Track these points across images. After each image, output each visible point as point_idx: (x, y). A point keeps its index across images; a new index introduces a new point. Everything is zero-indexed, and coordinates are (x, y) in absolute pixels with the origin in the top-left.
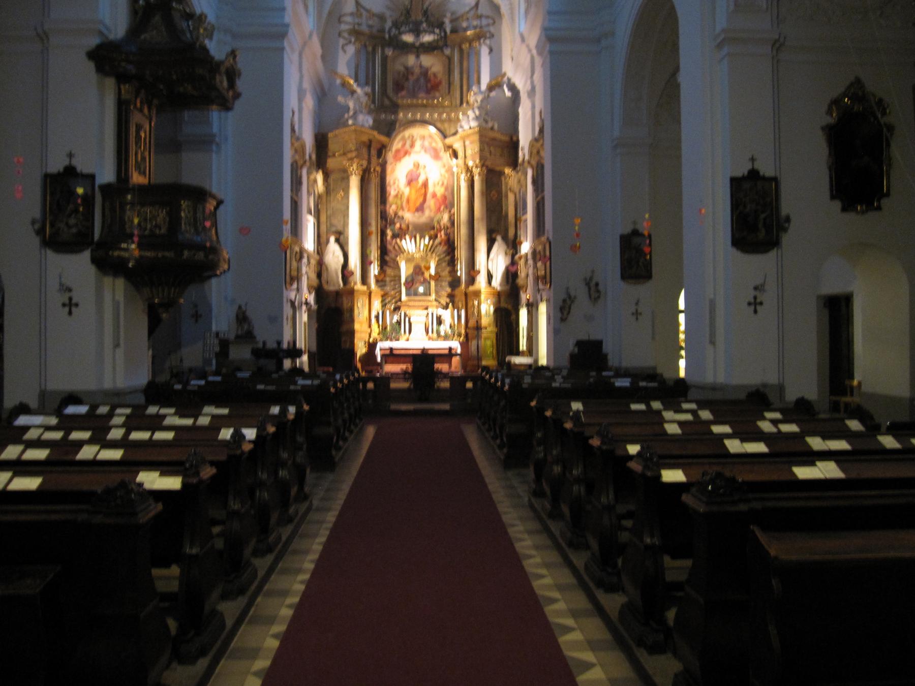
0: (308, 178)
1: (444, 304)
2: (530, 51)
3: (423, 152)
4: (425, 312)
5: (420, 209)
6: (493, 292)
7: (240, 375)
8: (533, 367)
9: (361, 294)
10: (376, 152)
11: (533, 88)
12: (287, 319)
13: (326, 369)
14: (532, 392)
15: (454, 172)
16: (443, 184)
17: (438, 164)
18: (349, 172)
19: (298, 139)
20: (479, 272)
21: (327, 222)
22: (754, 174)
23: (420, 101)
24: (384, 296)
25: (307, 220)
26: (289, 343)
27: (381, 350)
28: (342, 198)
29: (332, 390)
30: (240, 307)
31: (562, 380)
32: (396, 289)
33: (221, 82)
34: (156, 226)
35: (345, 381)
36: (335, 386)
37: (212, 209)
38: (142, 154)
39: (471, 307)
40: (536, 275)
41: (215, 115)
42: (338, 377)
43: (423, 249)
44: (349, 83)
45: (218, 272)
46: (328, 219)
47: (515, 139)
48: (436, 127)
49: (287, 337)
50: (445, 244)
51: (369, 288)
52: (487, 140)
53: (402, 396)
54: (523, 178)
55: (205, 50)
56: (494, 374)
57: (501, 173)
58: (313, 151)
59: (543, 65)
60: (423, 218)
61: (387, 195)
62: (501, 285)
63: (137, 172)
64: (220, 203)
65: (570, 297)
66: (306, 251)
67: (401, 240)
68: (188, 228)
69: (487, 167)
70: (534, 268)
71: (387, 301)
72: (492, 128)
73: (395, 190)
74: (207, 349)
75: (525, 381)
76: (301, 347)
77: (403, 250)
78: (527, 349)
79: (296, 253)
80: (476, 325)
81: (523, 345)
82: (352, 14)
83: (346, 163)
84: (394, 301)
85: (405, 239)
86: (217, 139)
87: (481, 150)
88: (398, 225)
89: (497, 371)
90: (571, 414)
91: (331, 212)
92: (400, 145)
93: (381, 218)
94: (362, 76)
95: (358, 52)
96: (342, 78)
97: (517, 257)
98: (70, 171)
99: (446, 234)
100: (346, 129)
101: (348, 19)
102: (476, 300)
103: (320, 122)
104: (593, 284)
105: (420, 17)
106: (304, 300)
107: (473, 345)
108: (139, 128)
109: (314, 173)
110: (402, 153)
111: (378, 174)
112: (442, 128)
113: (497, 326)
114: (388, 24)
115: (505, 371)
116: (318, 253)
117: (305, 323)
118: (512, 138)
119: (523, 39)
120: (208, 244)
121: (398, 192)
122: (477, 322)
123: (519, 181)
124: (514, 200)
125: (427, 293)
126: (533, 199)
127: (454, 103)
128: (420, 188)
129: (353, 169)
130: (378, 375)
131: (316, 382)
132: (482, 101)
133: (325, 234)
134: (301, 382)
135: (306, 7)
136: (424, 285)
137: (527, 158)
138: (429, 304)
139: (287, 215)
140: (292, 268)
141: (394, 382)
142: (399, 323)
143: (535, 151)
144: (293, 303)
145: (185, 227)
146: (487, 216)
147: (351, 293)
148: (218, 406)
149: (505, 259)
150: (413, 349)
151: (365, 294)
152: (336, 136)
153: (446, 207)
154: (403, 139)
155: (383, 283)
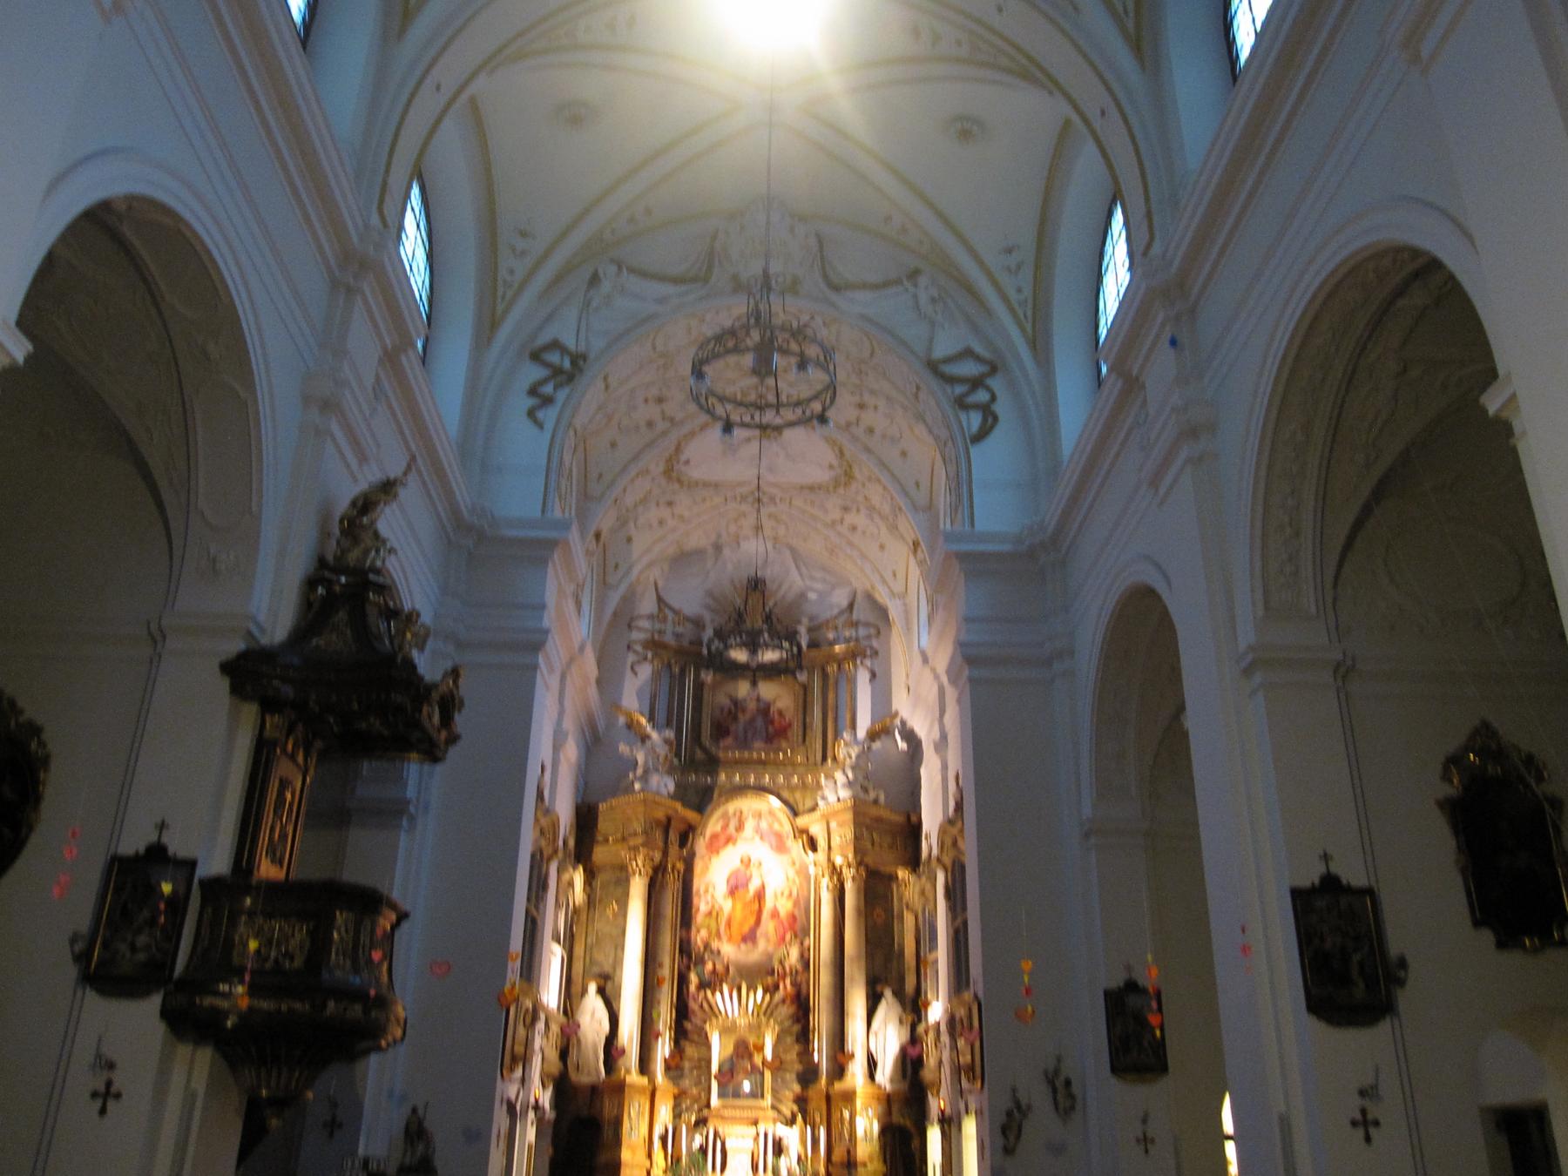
1: (788, 1113)
2: (937, 677)
3: (757, 838)
5: (750, 937)
16: (790, 895)
17: (784, 859)
19: (547, 812)
22: (1330, 883)
24: (678, 1099)
28: (615, 915)
33: (430, 717)
38: (283, 828)
41: (413, 769)
47: (914, 819)
50: (792, 1002)
51: (652, 1081)
52: (868, 821)
54: (928, 887)
57: (893, 878)
59: (959, 701)
60: (752, 955)
61: (694, 910)
62: (892, 1081)
63: (269, 860)
64: (403, 916)
65: (1019, 1106)
70: (951, 1049)
72: (876, 802)
73: (707, 903)
77: (717, 1012)
80: (846, 1160)
82: (651, 617)
83: (624, 854)
86: (412, 809)
87: (857, 838)
88: (709, 966)
92: (718, 828)
94: (661, 715)
95: (656, 676)
96: (629, 715)
98: (157, 854)
101: (645, 624)
103: (586, 783)
104: (1059, 1083)
105: (759, 623)
108: (284, 784)
112: (791, 800)
113: (885, 1161)
114: (709, 633)
119: (925, 660)
121: (713, 907)
123: (923, 893)
125: (757, 1094)
132: (858, 757)
137: (935, 852)
139: (516, 943)
142: (703, 1150)
143: (948, 842)
151: (644, 1093)
154: (726, 817)
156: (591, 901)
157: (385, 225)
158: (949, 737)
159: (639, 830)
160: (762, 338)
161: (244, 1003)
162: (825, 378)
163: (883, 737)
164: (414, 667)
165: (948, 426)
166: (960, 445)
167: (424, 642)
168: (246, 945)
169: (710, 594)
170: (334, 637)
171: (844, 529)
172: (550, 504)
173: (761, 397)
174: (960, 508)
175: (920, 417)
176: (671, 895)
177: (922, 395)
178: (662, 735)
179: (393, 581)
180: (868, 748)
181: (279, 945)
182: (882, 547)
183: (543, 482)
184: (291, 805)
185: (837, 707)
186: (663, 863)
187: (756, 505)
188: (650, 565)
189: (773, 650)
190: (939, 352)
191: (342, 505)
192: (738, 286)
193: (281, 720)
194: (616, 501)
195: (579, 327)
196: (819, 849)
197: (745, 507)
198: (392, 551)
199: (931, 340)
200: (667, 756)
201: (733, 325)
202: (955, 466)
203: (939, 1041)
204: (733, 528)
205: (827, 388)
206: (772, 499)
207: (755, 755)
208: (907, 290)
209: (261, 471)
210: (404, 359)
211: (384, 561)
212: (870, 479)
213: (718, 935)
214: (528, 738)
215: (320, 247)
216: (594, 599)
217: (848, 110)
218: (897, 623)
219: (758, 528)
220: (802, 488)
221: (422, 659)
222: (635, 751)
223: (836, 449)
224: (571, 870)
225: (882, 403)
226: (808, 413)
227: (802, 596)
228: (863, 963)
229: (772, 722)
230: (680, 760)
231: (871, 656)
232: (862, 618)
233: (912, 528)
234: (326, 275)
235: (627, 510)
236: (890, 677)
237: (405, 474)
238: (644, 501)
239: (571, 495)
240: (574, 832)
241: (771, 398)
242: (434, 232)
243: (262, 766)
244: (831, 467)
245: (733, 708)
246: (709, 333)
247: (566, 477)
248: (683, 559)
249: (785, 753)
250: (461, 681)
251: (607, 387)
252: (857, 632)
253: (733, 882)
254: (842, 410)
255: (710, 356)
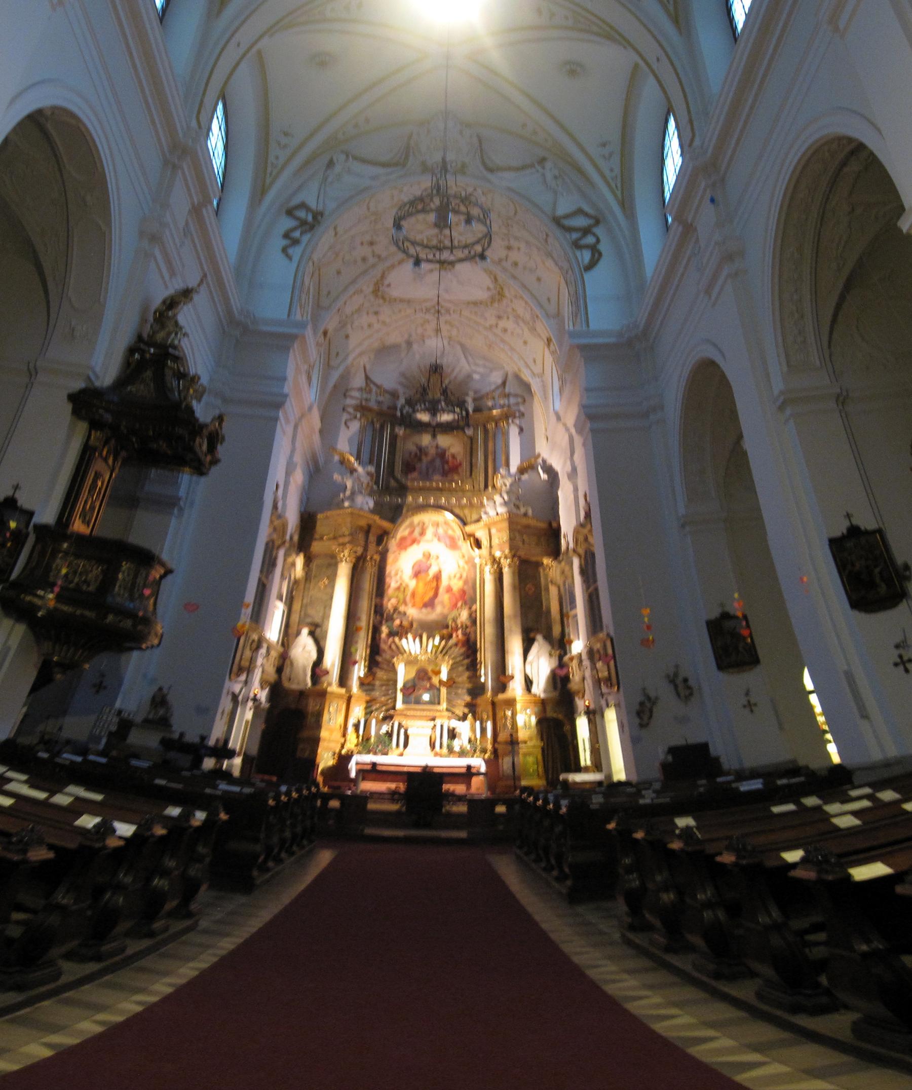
0: (285, 560)
1: (461, 714)
2: (567, 429)
3: (436, 540)
4: (432, 723)
5: (430, 604)
6: (535, 700)
7: (134, 762)
8: (605, 784)
9: (336, 697)
10: (375, 539)
11: (574, 469)
12: (223, 713)
13: (266, 777)
14: (607, 813)
15: (476, 564)
16: (461, 577)
17: (456, 554)
18: (338, 558)
19: (279, 517)
20: (512, 677)
21: (301, 611)
22: (854, 531)
23: (434, 484)
24: (369, 704)
25: (275, 607)
26: (218, 740)
27: (357, 764)
28: (326, 586)
29: (271, 802)
30: (160, 689)
31: (654, 795)
32: (388, 694)
33: (201, 446)
34: (85, 581)
35: (294, 795)
36: (277, 798)
37: (158, 576)
38: (93, 503)
39: (502, 718)
40: (597, 677)
41: (186, 478)
42: (284, 788)
43: (432, 651)
44: (348, 460)
45: (144, 646)
46: (303, 608)
47: (554, 525)
48: (452, 512)
49: (216, 733)
50: (463, 645)
51: (349, 690)
52: (519, 527)
53: (384, 819)
54: (567, 568)
55: (191, 412)
56: (541, 796)
57: (539, 564)
58: (295, 532)
59: (584, 445)
60: (432, 615)
61: (386, 587)
62: (545, 691)
63: (81, 520)
64: (168, 572)
65: (649, 698)
66: (267, 641)
67: (400, 639)
68: (122, 592)
69: (519, 557)
70: (592, 670)
71: (374, 708)
72: (525, 515)
73: (397, 582)
74: (100, 724)
75: (594, 801)
76: (236, 748)
77: (403, 651)
78: (592, 763)
79: (253, 641)
80: (509, 739)
81: (585, 758)
82: (360, 389)
83: (335, 548)
84: (384, 708)
85: (407, 638)
86: (182, 503)
87: (512, 539)
88: (397, 622)
89: (546, 792)
90: (677, 832)
91: (309, 601)
92: (406, 533)
93: (376, 612)
94: (365, 456)
95: (362, 430)
96: (342, 456)
97: (566, 658)
99: (464, 634)
100: (341, 512)
101: (356, 394)
102: (509, 710)
103: (308, 499)
104: (679, 680)
105: (438, 395)
106: (252, 695)
107: (506, 764)
108: (97, 476)
109: (294, 556)
110: (409, 541)
111: (375, 563)
112: (462, 515)
113: (542, 739)
114: (401, 401)
115: (559, 791)
116: (283, 644)
117: (247, 722)
118: (550, 524)
119: (559, 418)
120: (141, 614)
121: (401, 584)
122: (511, 735)
123: (563, 572)
124: (557, 593)
125: (435, 701)
126: (583, 592)
127: (476, 487)
128: (429, 582)
129: (344, 556)
130: (349, 793)
131: (247, 790)
132: (511, 485)
133: (296, 625)
134: (223, 786)
135: (309, 379)
136: (431, 692)
137: (571, 545)
138: (438, 714)
139: (250, 596)
140: (243, 657)
141: (375, 802)
142: (389, 735)
143: (581, 538)
144: (235, 697)
145: (119, 590)
146: (521, 613)
147: (322, 695)
148: (89, 787)
149: (549, 663)
150: (408, 766)
151: (342, 698)
152: (327, 517)
153: (465, 603)
154: (412, 526)
155: (370, 687)
156: (308, 575)
157: (200, 127)
158: (578, 469)
159: (347, 533)
160: (441, 203)
161: (52, 604)
162: (484, 229)
163: (529, 471)
164: (193, 412)
165: (569, 261)
166: (577, 272)
167: (202, 396)
168: (59, 571)
169: (403, 375)
170: (142, 387)
171: (498, 331)
172: (294, 310)
173: (440, 242)
174: (579, 314)
175: (549, 255)
176: (369, 577)
177: (550, 240)
178: (366, 469)
179: (184, 354)
180: (519, 479)
181: (81, 574)
182: (525, 343)
183: (290, 296)
184: (100, 489)
185: (495, 452)
186: (364, 556)
187: (437, 315)
188: (361, 354)
189: (448, 413)
190: (560, 212)
191: (157, 302)
192: (425, 169)
193: (101, 435)
194: (339, 310)
195: (319, 195)
196: (483, 547)
197: (428, 316)
198: (185, 335)
199: (555, 204)
200: (368, 483)
201: (422, 195)
202: (574, 287)
203: (582, 665)
204: (420, 331)
205: (485, 236)
206: (448, 311)
207: (434, 484)
208: (538, 171)
209: (108, 276)
210: (204, 211)
211: (179, 341)
212: (516, 297)
213: (405, 602)
214: (268, 466)
215: (159, 140)
216: (320, 376)
217: (496, 58)
218: (538, 394)
219: (438, 331)
220: (468, 303)
221: (199, 407)
222: (345, 480)
223: (492, 277)
224: (294, 557)
225: (523, 246)
226: (472, 253)
227: (469, 377)
228: (519, 619)
229: (447, 462)
230: (378, 487)
231: (519, 417)
232: (512, 391)
233: (546, 329)
234: (161, 157)
235: (347, 317)
236: (534, 430)
237: (199, 285)
238: (358, 310)
239: (309, 305)
240: (298, 532)
241: (447, 243)
242: (230, 131)
243: (85, 462)
244: (489, 289)
245: (418, 453)
246: (406, 200)
247: (305, 293)
248: (384, 351)
249: (457, 483)
250: (224, 424)
251: (336, 234)
252: (509, 401)
253: (416, 568)
254: (496, 251)
255: (406, 214)
